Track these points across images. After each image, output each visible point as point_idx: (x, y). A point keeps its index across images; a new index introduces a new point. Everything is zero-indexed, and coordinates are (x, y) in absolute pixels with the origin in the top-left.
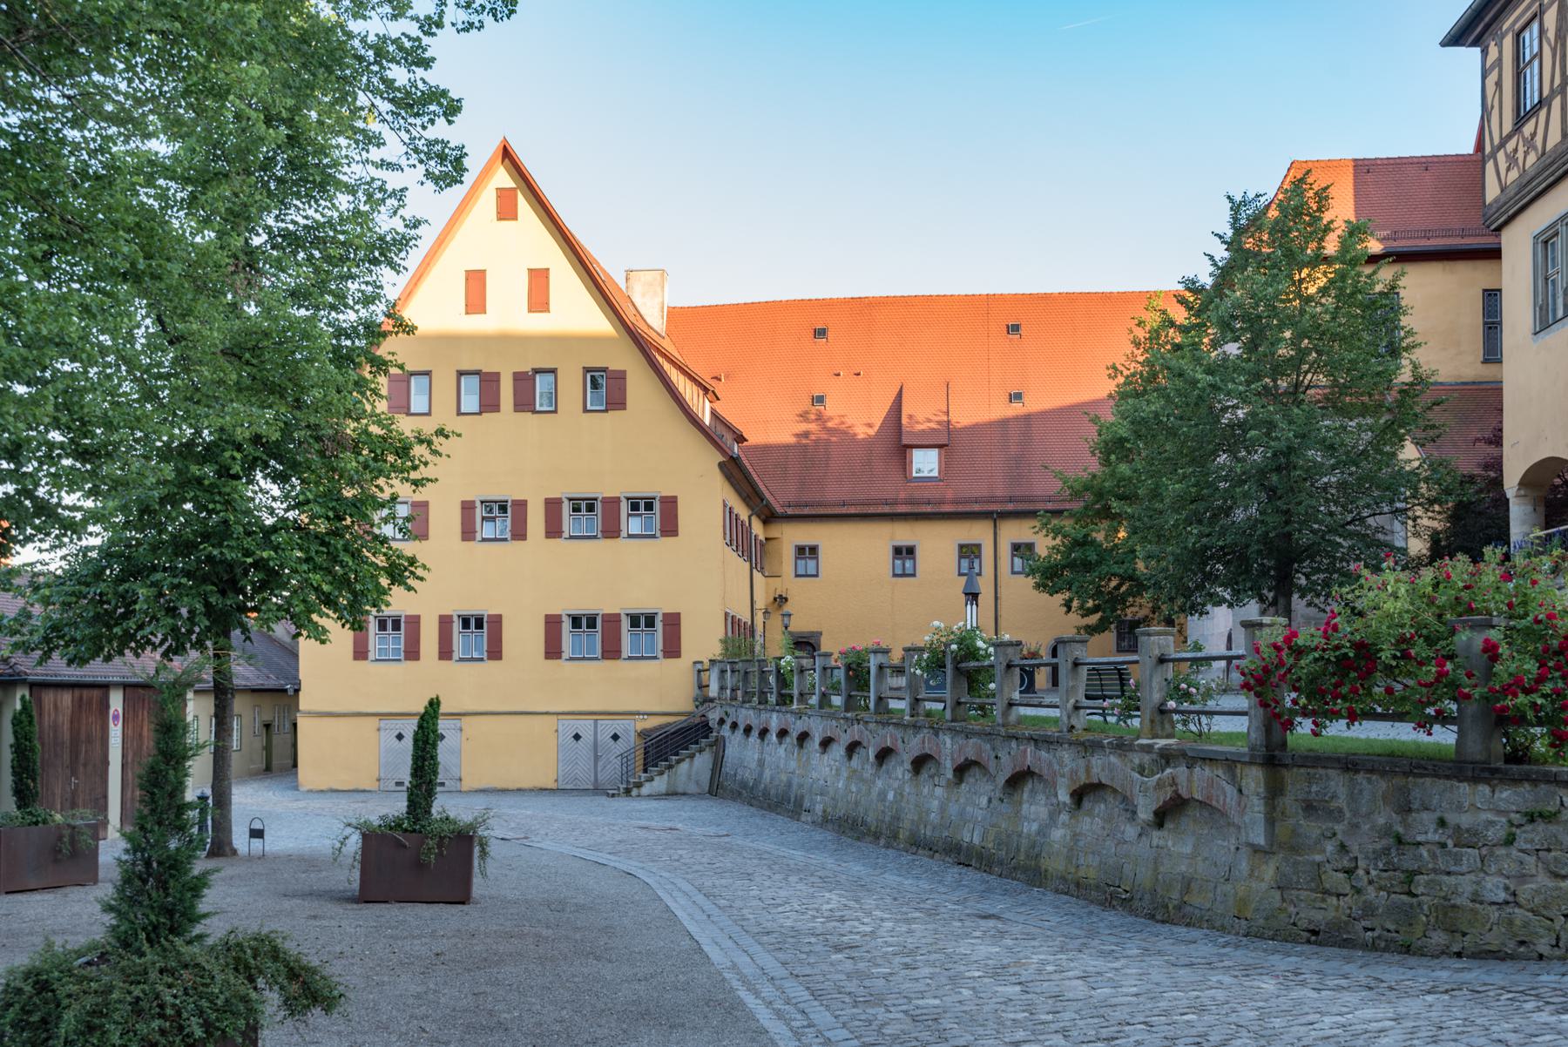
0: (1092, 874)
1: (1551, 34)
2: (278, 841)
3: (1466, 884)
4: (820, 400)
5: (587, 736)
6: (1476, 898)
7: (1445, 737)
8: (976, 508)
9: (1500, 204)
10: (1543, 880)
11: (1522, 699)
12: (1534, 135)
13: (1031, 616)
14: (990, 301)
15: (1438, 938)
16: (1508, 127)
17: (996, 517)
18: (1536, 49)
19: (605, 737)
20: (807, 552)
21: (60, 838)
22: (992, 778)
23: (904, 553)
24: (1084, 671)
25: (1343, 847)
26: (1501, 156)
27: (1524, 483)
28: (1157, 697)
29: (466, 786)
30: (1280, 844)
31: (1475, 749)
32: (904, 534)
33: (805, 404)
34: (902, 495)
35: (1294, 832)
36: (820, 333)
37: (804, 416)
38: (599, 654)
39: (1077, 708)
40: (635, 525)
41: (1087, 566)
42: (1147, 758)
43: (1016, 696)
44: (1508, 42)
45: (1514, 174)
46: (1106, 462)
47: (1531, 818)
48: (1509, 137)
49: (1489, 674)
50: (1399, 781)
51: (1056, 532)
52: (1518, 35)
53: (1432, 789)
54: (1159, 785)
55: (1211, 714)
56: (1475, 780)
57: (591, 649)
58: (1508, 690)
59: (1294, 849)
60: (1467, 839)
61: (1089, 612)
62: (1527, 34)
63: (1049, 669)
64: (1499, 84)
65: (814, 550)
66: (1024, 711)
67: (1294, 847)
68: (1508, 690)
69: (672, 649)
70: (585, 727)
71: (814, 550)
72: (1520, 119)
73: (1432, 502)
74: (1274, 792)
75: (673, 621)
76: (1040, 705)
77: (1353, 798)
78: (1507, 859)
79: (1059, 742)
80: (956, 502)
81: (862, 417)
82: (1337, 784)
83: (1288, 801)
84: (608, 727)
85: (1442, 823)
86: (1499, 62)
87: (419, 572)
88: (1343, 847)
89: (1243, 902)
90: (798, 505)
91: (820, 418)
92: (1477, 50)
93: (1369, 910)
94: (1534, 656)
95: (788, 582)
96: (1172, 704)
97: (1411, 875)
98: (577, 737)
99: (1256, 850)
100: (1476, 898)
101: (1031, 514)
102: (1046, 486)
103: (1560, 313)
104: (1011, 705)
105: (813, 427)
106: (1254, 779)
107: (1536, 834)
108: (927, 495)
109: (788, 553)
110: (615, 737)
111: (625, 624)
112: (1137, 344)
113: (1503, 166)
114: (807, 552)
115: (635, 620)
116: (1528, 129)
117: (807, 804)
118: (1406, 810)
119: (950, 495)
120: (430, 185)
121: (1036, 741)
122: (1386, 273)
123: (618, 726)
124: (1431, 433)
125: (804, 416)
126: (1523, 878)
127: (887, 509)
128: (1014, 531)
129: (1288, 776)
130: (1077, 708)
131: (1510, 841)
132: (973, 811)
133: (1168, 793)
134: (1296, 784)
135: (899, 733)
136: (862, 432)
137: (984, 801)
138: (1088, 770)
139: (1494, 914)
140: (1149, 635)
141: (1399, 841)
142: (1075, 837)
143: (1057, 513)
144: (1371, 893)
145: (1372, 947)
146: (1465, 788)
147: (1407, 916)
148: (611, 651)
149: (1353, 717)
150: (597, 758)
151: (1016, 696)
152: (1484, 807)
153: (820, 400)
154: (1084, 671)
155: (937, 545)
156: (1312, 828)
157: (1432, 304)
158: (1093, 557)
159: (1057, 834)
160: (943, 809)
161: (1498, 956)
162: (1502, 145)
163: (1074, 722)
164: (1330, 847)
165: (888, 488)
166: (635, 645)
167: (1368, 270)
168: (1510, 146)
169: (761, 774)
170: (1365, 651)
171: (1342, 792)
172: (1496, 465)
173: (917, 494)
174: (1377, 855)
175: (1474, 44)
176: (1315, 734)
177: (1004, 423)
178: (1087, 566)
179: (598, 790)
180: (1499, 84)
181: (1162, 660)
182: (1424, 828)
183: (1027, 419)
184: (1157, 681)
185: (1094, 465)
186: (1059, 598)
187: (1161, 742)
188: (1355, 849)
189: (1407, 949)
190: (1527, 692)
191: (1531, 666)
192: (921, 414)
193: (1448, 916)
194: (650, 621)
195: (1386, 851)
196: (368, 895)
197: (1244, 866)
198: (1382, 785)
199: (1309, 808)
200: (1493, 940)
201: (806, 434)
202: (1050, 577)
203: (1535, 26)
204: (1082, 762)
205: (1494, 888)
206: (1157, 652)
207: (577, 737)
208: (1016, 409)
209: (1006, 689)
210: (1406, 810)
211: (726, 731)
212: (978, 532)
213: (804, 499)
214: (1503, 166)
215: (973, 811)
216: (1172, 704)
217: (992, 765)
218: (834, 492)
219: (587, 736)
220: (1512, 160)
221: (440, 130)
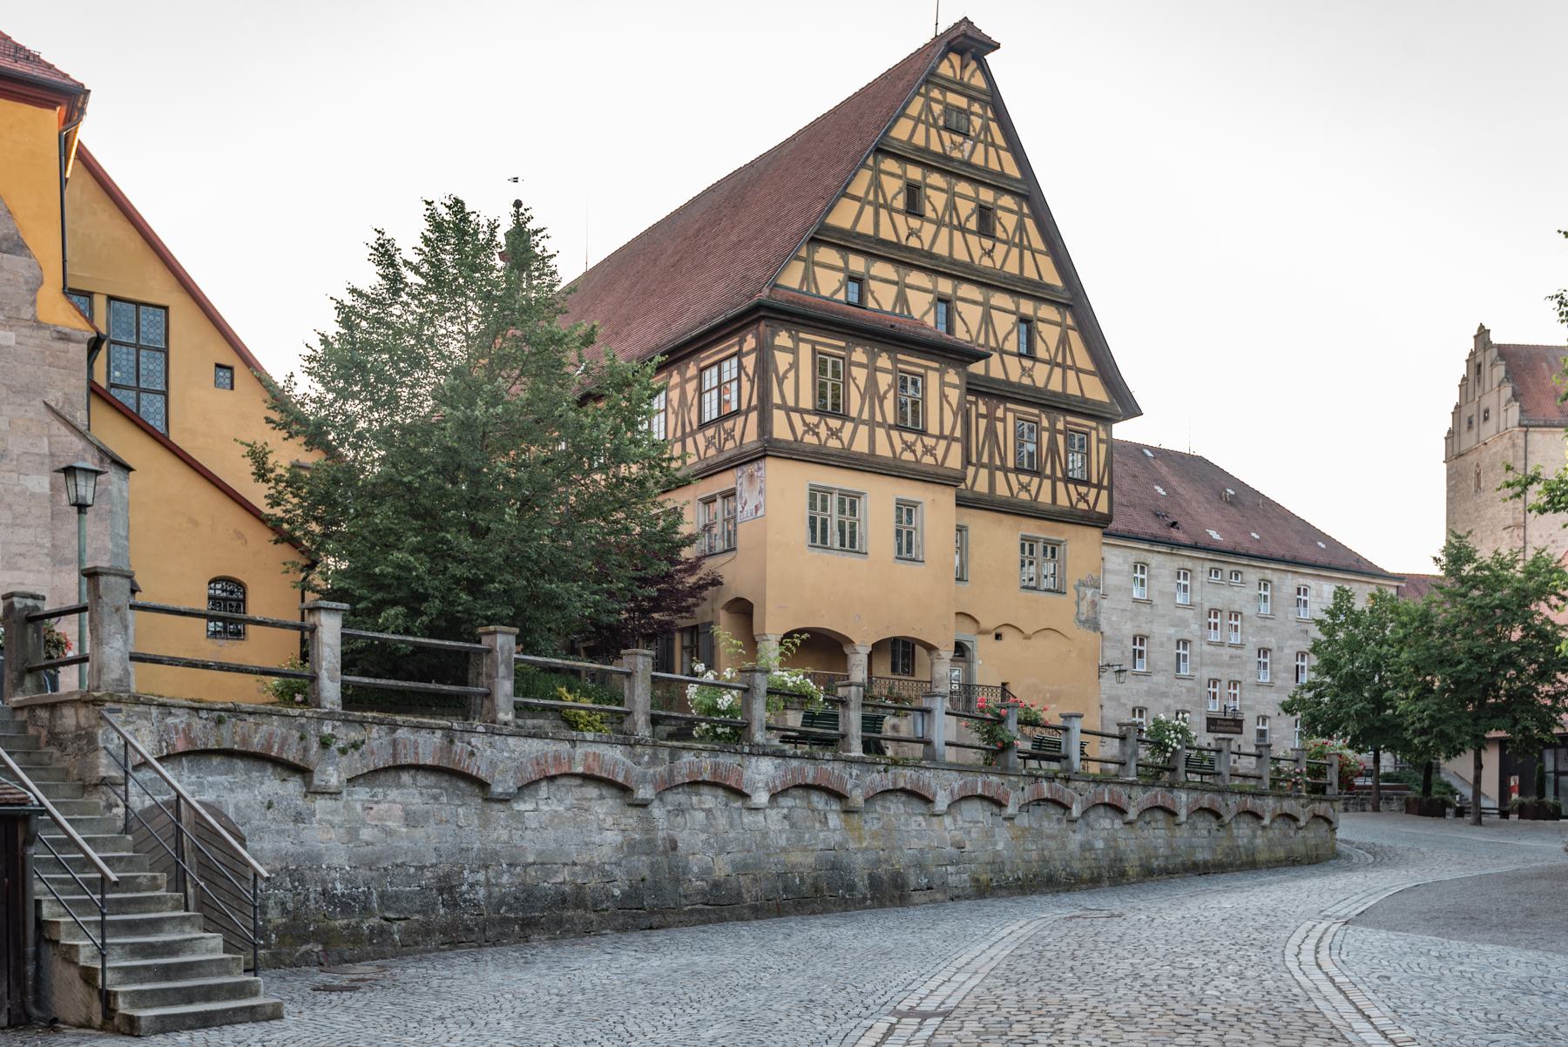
1: (675, 403)
18: (735, 375)
62: (707, 373)
137: (1205, 833)
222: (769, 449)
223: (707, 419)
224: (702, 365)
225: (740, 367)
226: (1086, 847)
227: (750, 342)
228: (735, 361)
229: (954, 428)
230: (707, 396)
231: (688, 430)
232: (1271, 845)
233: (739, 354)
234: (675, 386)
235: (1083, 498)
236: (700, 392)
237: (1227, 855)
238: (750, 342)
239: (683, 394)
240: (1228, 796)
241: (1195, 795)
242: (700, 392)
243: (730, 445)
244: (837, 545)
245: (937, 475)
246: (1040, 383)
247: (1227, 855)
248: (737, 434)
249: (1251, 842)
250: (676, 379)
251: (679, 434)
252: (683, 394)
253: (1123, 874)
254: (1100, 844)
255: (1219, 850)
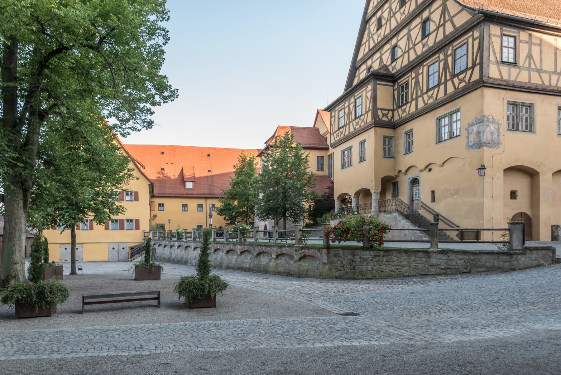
0: (282, 270)
1: (347, 113)
2: (84, 272)
3: (365, 268)
4: (163, 169)
5: (116, 248)
6: (366, 270)
7: (361, 244)
8: (202, 196)
10: (378, 266)
13: (218, 221)
14: (202, 149)
15: (360, 277)
16: (337, 129)
17: (206, 198)
19: (121, 248)
20: (161, 205)
21: (56, 269)
22: (253, 254)
23: (185, 206)
25: (342, 263)
26: (335, 134)
27: (338, 197)
28: (299, 237)
29: (84, 261)
30: (330, 262)
31: (366, 245)
32: (185, 201)
33: (160, 170)
34: (184, 193)
35: (332, 260)
36: (163, 153)
37: (158, 173)
38: (119, 228)
40: (127, 198)
41: (229, 209)
42: (297, 248)
44: (337, 112)
45: (338, 138)
46: (233, 187)
47: (376, 256)
50: (352, 251)
51: (223, 202)
52: (339, 112)
53: (359, 252)
54: (300, 253)
55: (307, 240)
56: (367, 250)
57: (116, 227)
59: (332, 263)
60: (365, 260)
61: (228, 220)
62: (341, 112)
64: (335, 120)
65: (163, 205)
67: (332, 263)
69: (137, 228)
70: (116, 246)
71: (163, 205)
72: (339, 128)
74: (328, 253)
75: (137, 221)
77: (343, 254)
78: (372, 263)
79: (273, 246)
80: (197, 194)
81: (173, 173)
82: (341, 252)
83: (331, 255)
84: (121, 246)
85: (360, 258)
86: (335, 116)
87: (124, 210)
88: (342, 263)
89: (321, 273)
90: (159, 194)
91: (163, 174)
93: (347, 273)
95: (156, 211)
97: (355, 267)
98: (113, 248)
99: (324, 263)
100: (366, 270)
101: (218, 198)
102: (218, 192)
104: (257, 239)
105: (161, 176)
106: (324, 251)
107: (377, 258)
108: (190, 193)
109: (157, 205)
110: (123, 248)
111: (125, 221)
112: (239, 161)
114: (161, 205)
115: (128, 221)
116: (341, 130)
117: (189, 261)
118: (354, 255)
119: (195, 193)
120: (145, 128)
121: (266, 246)
123: (124, 246)
125: (158, 173)
126: (374, 266)
127: (181, 196)
128: (210, 202)
129: (331, 251)
131: (372, 260)
132: (247, 260)
133: (303, 255)
134: (332, 252)
135: (222, 246)
136: (172, 177)
137: (249, 258)
138: (281, 251)
139: (369, 272)
141: (353, 261)
142: (277, 264)
143: (223, 198)
144: (347, 270)
145: (347, 279)
146: (365, 252)
147: (354, 273)
148: (122, 228)
149: (346, 240)
150: (118, 253)
152: (367, 255)
153: (163, 169)
155: (193, 204)
156: (336, 259)
158: (231, 208)
159: (271, 264)
160: (236, 261)
161: (370, 279)
162: (335, 132)
164: (339, 262)
165: (181, 191)
166: (128, 227)
168: (337, 133)
169: (171, 256)
170: (349, 229)
171: (342, 253)
172: (332, 194)
173: (188, 192)
174: (348, 263)
177: (207, 177)
178: (229, 209)
179: (119, 261)
180: (335, 120)
182: (357, 259)
183: (212, 176)
185: (230, 187)
186: (223, 217)
187: (301, 246)
188: (344, 262)
189: (354, 279)
191: (377, 232)
192: (187, 174)
193: (362, 273)
194: (132, 221)
195: (350, 263)
196: (135, 280)
197: (321, 267)
198: (349, 252)
199: (335, 256)
200: (369, 276)
201: (159, 177)
202: (221, 212)
203: (343, 110)
204: (279, 250)
205: (370, 268)
207: (113, 248)
208: (210, 174)
210: (354, 255)
211: (156, 246)
212: (202, 202)
213: (161, 192)
215: (247, 260)
217: (253, 251)
218: (168, 191)
219: (116, 248)
220: (337, 135)
221: (149, 117)
225: (344, 112)
226: (216, 259)
230: (358, 108)
232: (276, 266)
233: (344, 108)
237: (255, 267)
239: (349, 109)
240: (254, 247)
241: (243, 246)
242: (355, 107)
243: (363, 124)
244: (524, 129)
245: (438, 103)
247: (255, 267)
248: (365, 120)
249: (267, 263)
250: (347, 104)
252: (349, 109)
253: (221, 267)
254: (219, 259)
255: (252, 265)
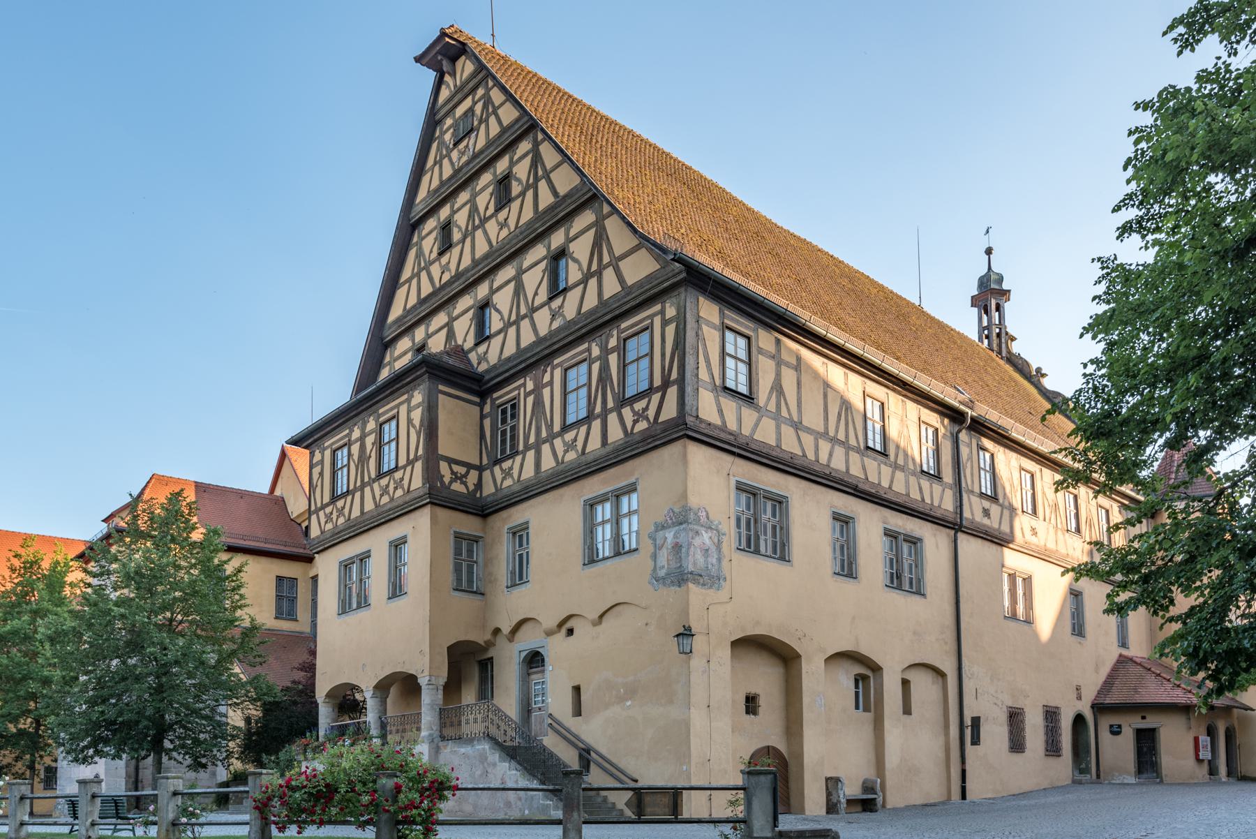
1: (356, 457)
9: (319, 540)
11: (414, 811)
12: (343, 508)
18: (345, 462)
24: (98, 801)
27: (328, 696)
28: (171, 816)
39: (93, 824)
43: (26, 818)
44: (328, 453)
45: (329, 526)
48: (327, 505)
49: (395, 800)
55: (202, 825)
58: (406, 808)
62: (339, 453)
63: (770, 777)
64: (321, 474)
66: (31, 829)
68: (406, 808)
72: (334, 498)
73: (255, 700)
76: (55, 824)
92: (307, 451)
94: (417, 791)
96: (184, 820)
103: (355, 606)
104: (22, 824)
112: (13, 570)
113: (323, 520)
116: (340, 504)
122: (237, 560)
124: (258, 660)
130: (93, 824)
140: (167, 778)
149: (322, 823)
151: (26, 818)
154: (98, 801)
157: (256, 584)
162: (323, 507)
163: (90, 834)
167: (224, 556)
175: (306, 447)
176: (299, 833)
180: (321, 474)
181: (175, 794)
184: (172, 807)
190: (417, 808)
206: (172, 789)
209: (19, 814)
214: (323, 520)
216: (184, 820)
220: (329, 518)
222: (684, 430)
223: (386, 469)
224: (381, 419)
225: (350, 455)
227: (418, 397)
228: (345, 450)
229: (837, 431)
230: (386, 448)
231: (366, 479)
233: (349, 444)
234: (356, 441)
235: (986, 513)
236: (380, 444)
238: (418, 397)
239: (363, 447)
242: (380, 444)
243: (399, 493)
246: (746, 431)
250: (356, 434)
251: (359, 484)
252: (363, 447)
